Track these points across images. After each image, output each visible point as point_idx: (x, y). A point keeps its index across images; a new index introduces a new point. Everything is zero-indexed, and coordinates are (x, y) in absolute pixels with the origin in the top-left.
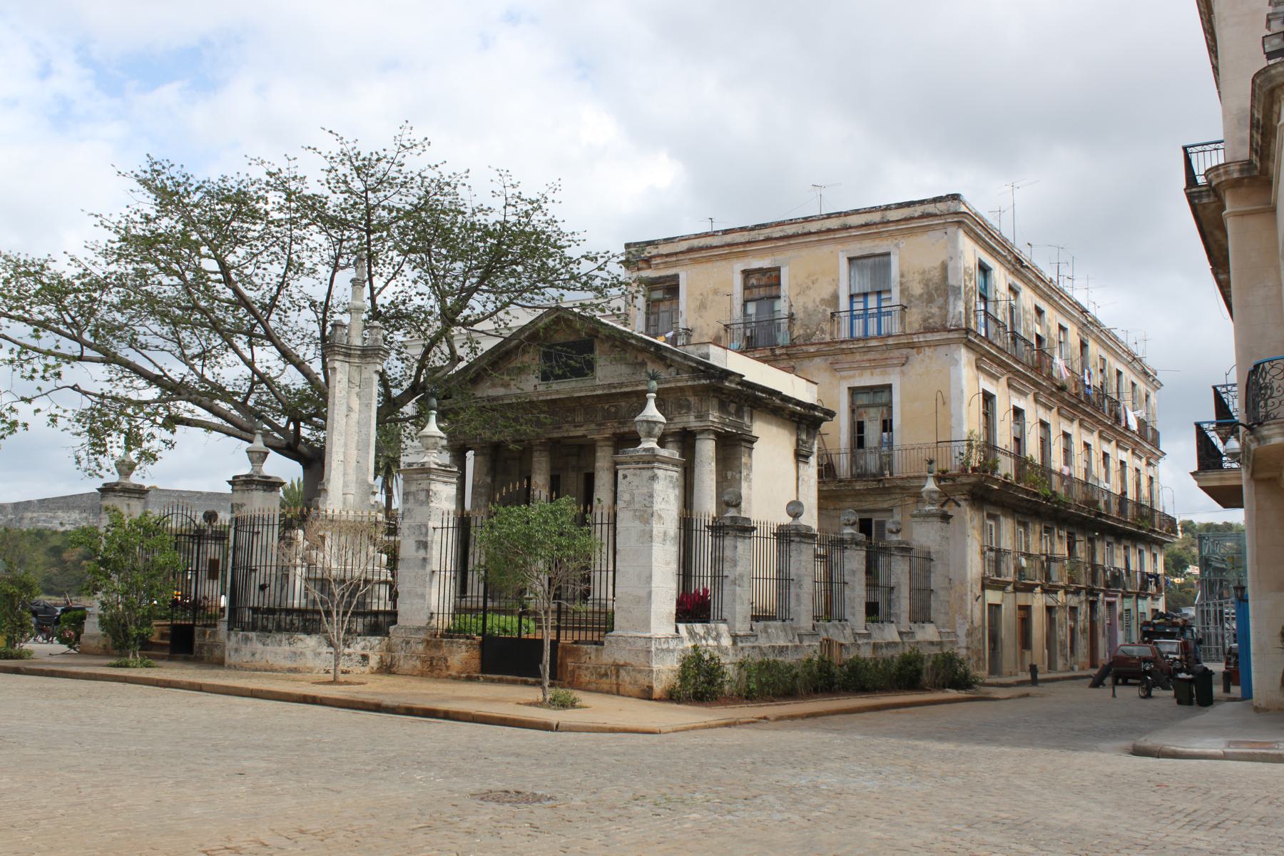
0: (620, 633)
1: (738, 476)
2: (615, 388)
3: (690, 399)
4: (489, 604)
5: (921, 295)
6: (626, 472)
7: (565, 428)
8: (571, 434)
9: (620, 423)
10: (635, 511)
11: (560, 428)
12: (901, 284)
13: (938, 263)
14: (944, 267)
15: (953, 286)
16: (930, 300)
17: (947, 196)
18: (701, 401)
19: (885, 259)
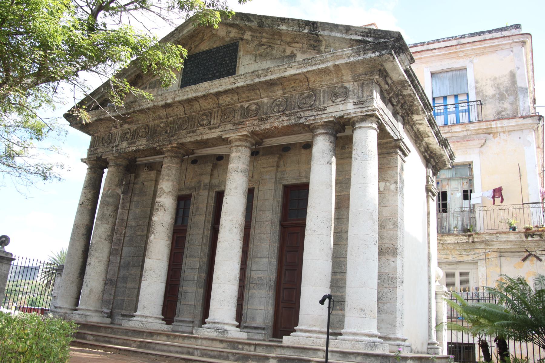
1: (393, 187)
2: (259, 76)
4: (330, 331)
5: (494, 95)
7: (198, 132)
8: (205, 137)
9: (261, 120)
11: (193, 132)
12: (476, 88)
13: (507, 72)
14: (513, 75)
15: (522, 88)
16: (502, 97)
17: (512, 26)
19: (464, 71)
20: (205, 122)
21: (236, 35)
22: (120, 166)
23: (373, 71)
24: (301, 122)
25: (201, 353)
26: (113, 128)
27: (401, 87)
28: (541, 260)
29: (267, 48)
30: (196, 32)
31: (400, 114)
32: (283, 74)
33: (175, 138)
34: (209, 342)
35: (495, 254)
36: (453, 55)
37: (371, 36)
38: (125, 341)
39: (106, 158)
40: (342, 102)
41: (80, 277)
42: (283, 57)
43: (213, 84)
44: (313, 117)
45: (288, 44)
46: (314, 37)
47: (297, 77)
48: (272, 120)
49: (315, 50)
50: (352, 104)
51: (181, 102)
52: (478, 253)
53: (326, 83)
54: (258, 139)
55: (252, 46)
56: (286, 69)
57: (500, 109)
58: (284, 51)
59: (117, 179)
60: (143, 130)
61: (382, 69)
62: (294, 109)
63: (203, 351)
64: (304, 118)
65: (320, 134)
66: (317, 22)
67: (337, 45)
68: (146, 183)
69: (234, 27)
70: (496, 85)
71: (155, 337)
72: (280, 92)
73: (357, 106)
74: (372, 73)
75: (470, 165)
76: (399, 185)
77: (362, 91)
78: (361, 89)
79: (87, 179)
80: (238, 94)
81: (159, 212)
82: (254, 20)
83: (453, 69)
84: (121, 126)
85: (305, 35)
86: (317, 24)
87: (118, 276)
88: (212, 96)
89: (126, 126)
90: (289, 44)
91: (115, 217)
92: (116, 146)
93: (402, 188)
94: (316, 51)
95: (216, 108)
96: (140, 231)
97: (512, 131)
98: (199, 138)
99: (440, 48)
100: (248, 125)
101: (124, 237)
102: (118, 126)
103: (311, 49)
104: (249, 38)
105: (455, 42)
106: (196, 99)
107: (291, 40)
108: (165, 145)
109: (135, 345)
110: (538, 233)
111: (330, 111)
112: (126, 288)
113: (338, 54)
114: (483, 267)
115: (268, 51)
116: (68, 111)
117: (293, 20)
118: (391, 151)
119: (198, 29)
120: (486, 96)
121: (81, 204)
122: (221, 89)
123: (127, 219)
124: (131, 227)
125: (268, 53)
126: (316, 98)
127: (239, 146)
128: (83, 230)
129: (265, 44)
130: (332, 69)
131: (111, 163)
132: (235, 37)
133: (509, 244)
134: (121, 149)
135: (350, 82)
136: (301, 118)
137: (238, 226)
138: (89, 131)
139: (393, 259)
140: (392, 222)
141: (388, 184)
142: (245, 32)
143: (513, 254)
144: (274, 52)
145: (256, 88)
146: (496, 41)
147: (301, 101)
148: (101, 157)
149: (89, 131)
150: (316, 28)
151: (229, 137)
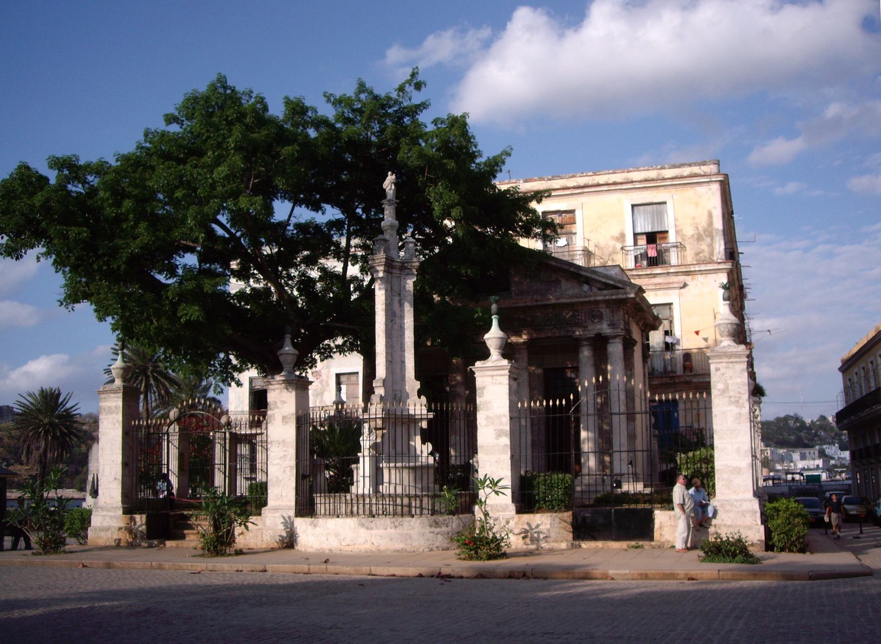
0: (723, 497)
3: (603, 310)
5: (693, 236)
6: (718, 366)
10: (730, 397)
12: (676, 226)
18: (612, 312)
57: (698, 250)
77: (613, 316)
116: (59, 164)
120: (685, 236)
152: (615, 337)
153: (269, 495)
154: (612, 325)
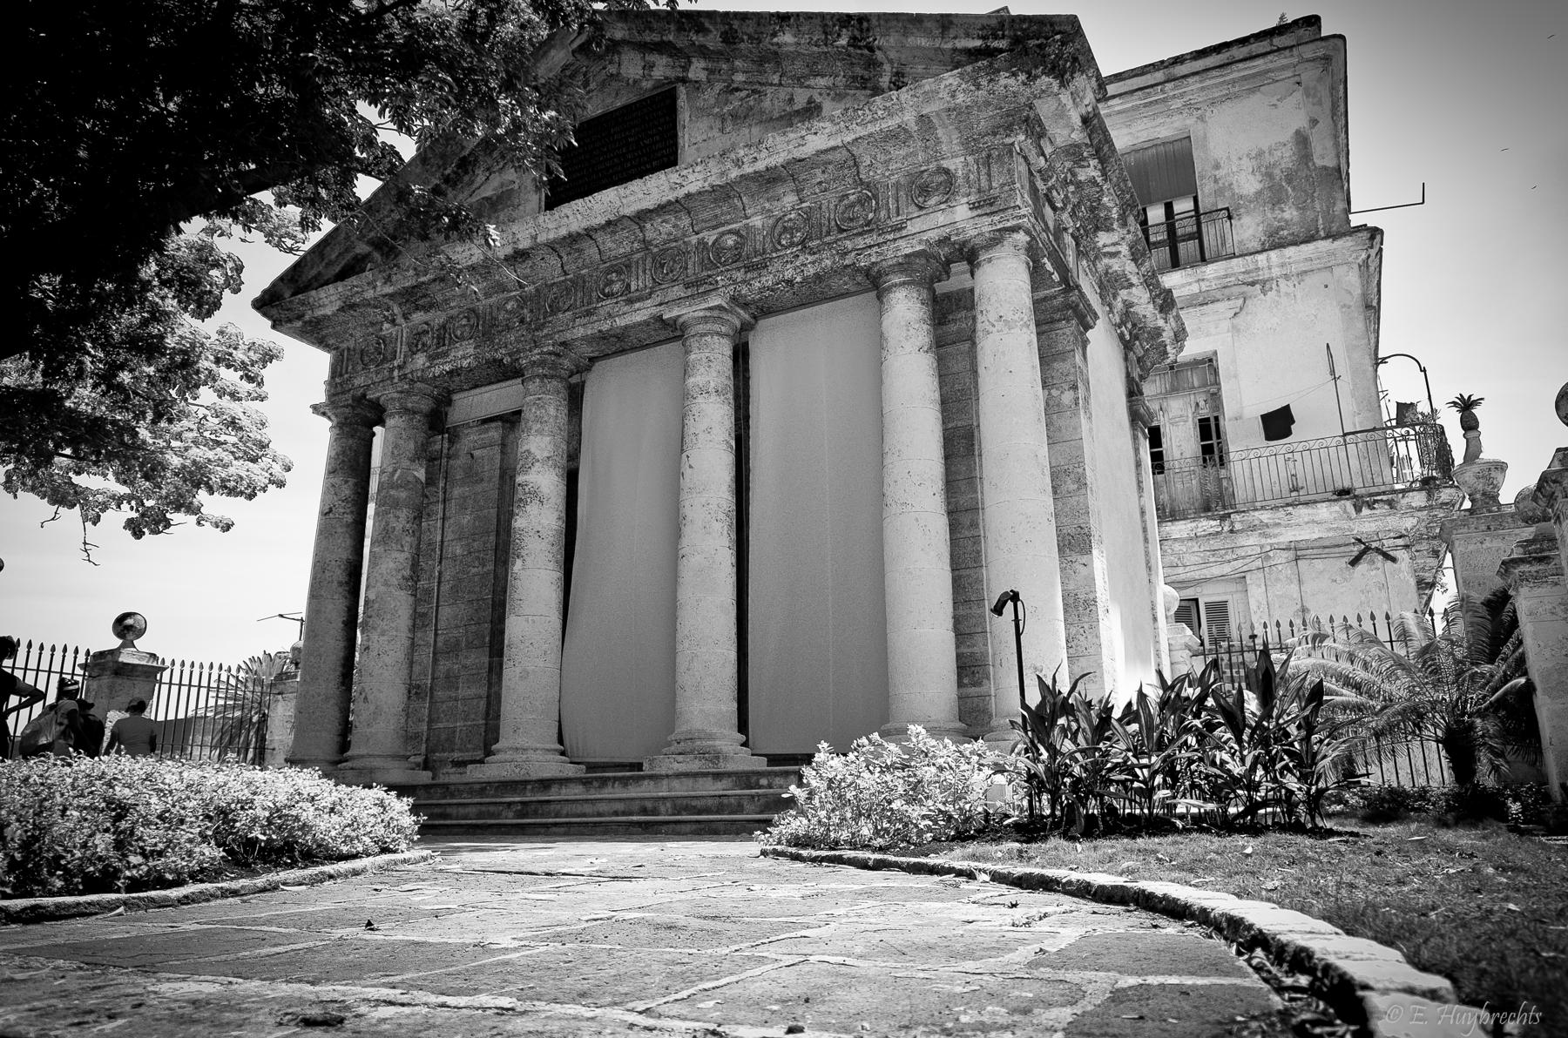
1: (1067, 397)
5: (1259, 193)
8: (621, 322)
11: (589, 313)
17: (1295, 22)
20: (616, 287)
21: (671, 74)
22: (415, 413)
23: (1012, 124)
24: (847, 262)
25: (674, 806)
26: (386, 325)
27: (1075, 163)
28: (1394, 560)
29: (748, 96)
30: (568, 73)
31: (1070, 231)
32: (798, 154)
33: (545, 331)
34: (689, 782)
35: (1285, 554)
36: (1160, 108)
37: (1003, 37)
38: (483, 808)
39: (378, 398)
40: (943, 206)
41: (343, 684)
42: (790, 114)
43: (628, 192)
44: (875, 249)
45: (799, 80)
46: (862, 55)
47: (830, 157)
48: (778, 265)
49: (865, 88)
50: (966, 207)
51: (552, 246)
52: (1243, 558)
53: (899, 165)
54: (747, 316)
55: (709, 96)
56: (803, 137)
58: (791, 100)
59: (412, 445)
60: (464, 322)
61: (1032, 116)
62: (828, 233)
63: (679, 802)
64: (853, 254)
65: (895, 285)
66: (870, 14)
67: (920, 68)
68: (477, 453)
69: (661, 53)
70: (1263, 169)
71: (554, 789)
72: (790, 199)
73: (979, 212)
74: (1009, 129)
75: (1211, 360)
76: (1081, 392)
77: (989, 175)
78: (984, 171)
79: (334, 453)
80: (689, 213)
81: (528, 508)
82: (711, 27)
83: (1159, 142)
84: (406, 317)
85: (841, 53)
86: (868, 21)
87: (433, 674)
88: (627, 223)
89: (418, 317)
90: (800, 81)
91: (417, 534)
92: (400, 367)
93: (1086, 400)
94: (869, 92)
95: (638, 251)
96: (477, 564)
97: (1306, 272)
98: (605, 327)
99: (1125, 93)
100: (721, 283)
101: (439, 583)
102: (400, 320)
103: (857, 88)
104: (703, 76)
105: (1159, 76)
106: (589, 233)
107: (806, 71)
108: (524, 350)
109: (511, 814)
110: (1385, 498)
111: (914, 231)
112: (456, 700)
113: (927, 88)
114: (1259, 586)
115: (752, 103)
117: (810, 16)
118: (1057, 316)
119: (572, 65)
120: (1241, 197)
121: (326, 513)
122: (649, 204)
123: (442, 542)
124: (454, 558)
125: (751, 108)
126: (877, 203)
127: (705, 335)
128: (339, 574)
129: (741, 86)
130: (913, 127)
131: (391, 408)
132: (666, 78)
133: (1316, 530)
134: (412, 372)
135: (957, 156)
136: (846, 254)
137: (722, 516)
138: (324, 337)
139: (1084, 559)
140: (1072, 476)
141: (1055, 392)
142: (690, 63)
143: (1327, 550)
144: (767, 104)
145: (732, 194)
146: (1260, 62)
147: (843, 213)
148: (364, 396)
149: (324, 337)
150: (868, 30)
151: (679, 316)
152: (996, 240)
153: (949, 623)
154: (985, 204)
